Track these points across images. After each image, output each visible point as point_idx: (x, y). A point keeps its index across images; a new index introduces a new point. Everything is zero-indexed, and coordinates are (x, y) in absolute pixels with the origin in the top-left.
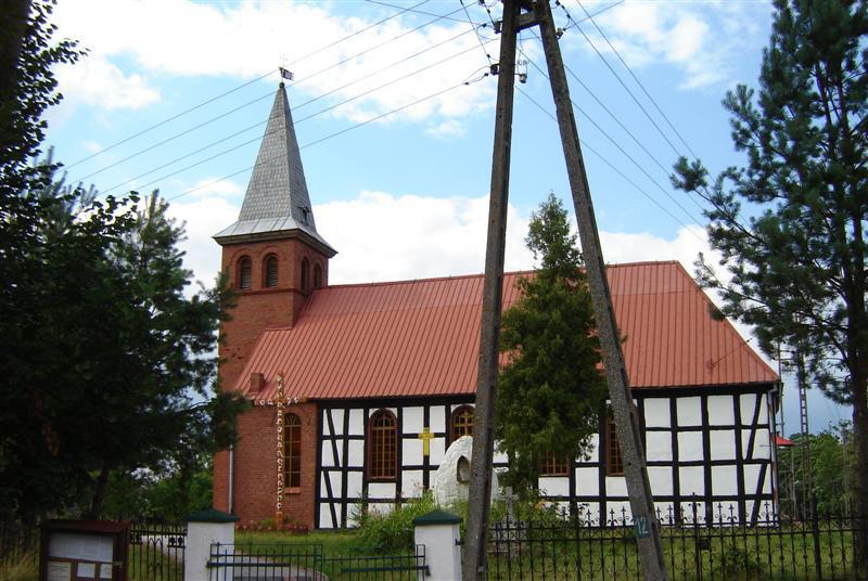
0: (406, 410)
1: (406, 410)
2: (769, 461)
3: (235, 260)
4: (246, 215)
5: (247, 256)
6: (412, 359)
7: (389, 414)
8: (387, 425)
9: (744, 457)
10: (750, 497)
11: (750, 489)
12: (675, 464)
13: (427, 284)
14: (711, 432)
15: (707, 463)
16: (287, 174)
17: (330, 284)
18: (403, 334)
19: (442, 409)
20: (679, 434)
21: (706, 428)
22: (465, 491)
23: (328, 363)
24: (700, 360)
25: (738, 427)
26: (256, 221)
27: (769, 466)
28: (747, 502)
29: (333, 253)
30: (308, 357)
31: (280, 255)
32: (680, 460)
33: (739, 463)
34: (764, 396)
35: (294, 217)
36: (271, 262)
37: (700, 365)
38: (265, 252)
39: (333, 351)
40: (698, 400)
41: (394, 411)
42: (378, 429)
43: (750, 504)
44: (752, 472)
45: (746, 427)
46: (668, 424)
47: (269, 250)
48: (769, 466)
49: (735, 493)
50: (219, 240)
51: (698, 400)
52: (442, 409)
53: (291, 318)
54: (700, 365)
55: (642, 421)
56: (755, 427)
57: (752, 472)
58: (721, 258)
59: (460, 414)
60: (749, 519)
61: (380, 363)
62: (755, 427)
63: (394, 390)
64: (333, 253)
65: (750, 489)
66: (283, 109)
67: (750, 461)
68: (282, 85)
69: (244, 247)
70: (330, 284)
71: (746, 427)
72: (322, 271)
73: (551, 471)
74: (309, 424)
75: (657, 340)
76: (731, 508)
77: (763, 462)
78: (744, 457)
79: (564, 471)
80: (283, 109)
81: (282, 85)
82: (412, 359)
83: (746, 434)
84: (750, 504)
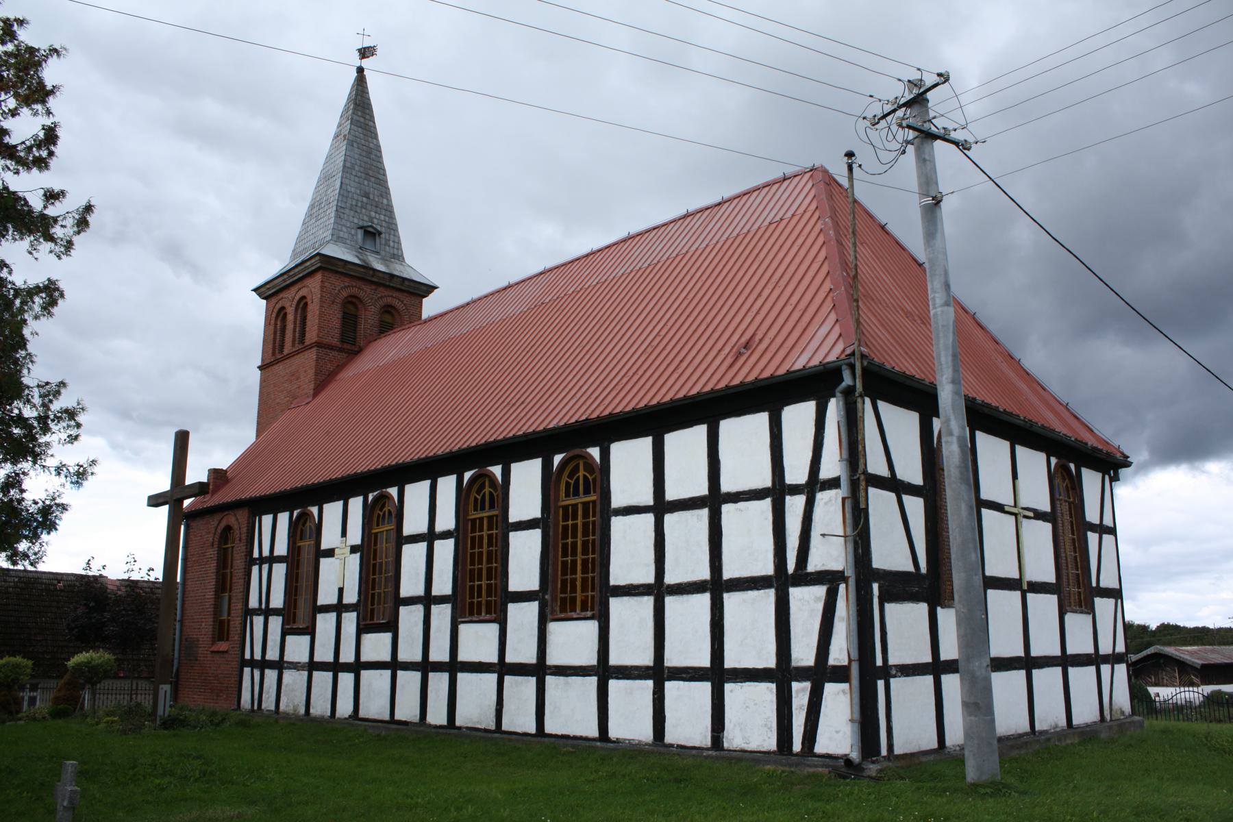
6: (495, 361)
9: (791, 566)
14: (331, 674)
23: (411, 400)
27: (842, 587)
28: (795, 686)
30: (476, 365)
32: (400, 673)
39: (509, 351)
45: (795, 490)
53: (312, 386)
56: (814, 485)
58: (53, 61)
60: (797, 746)
61: (407, 405)
62: (814, 485)
65: (804, 653)
66: (360, 102)
67: (804, 578)
68: (360, 70)
71: (795, 490)
74: (240, 540)
75: (627, 258)
76: (808, 659)
77: (830, 579)
78: (791, 566)
80: (360, 102)
81: (360, 70)
82: (495, 361)
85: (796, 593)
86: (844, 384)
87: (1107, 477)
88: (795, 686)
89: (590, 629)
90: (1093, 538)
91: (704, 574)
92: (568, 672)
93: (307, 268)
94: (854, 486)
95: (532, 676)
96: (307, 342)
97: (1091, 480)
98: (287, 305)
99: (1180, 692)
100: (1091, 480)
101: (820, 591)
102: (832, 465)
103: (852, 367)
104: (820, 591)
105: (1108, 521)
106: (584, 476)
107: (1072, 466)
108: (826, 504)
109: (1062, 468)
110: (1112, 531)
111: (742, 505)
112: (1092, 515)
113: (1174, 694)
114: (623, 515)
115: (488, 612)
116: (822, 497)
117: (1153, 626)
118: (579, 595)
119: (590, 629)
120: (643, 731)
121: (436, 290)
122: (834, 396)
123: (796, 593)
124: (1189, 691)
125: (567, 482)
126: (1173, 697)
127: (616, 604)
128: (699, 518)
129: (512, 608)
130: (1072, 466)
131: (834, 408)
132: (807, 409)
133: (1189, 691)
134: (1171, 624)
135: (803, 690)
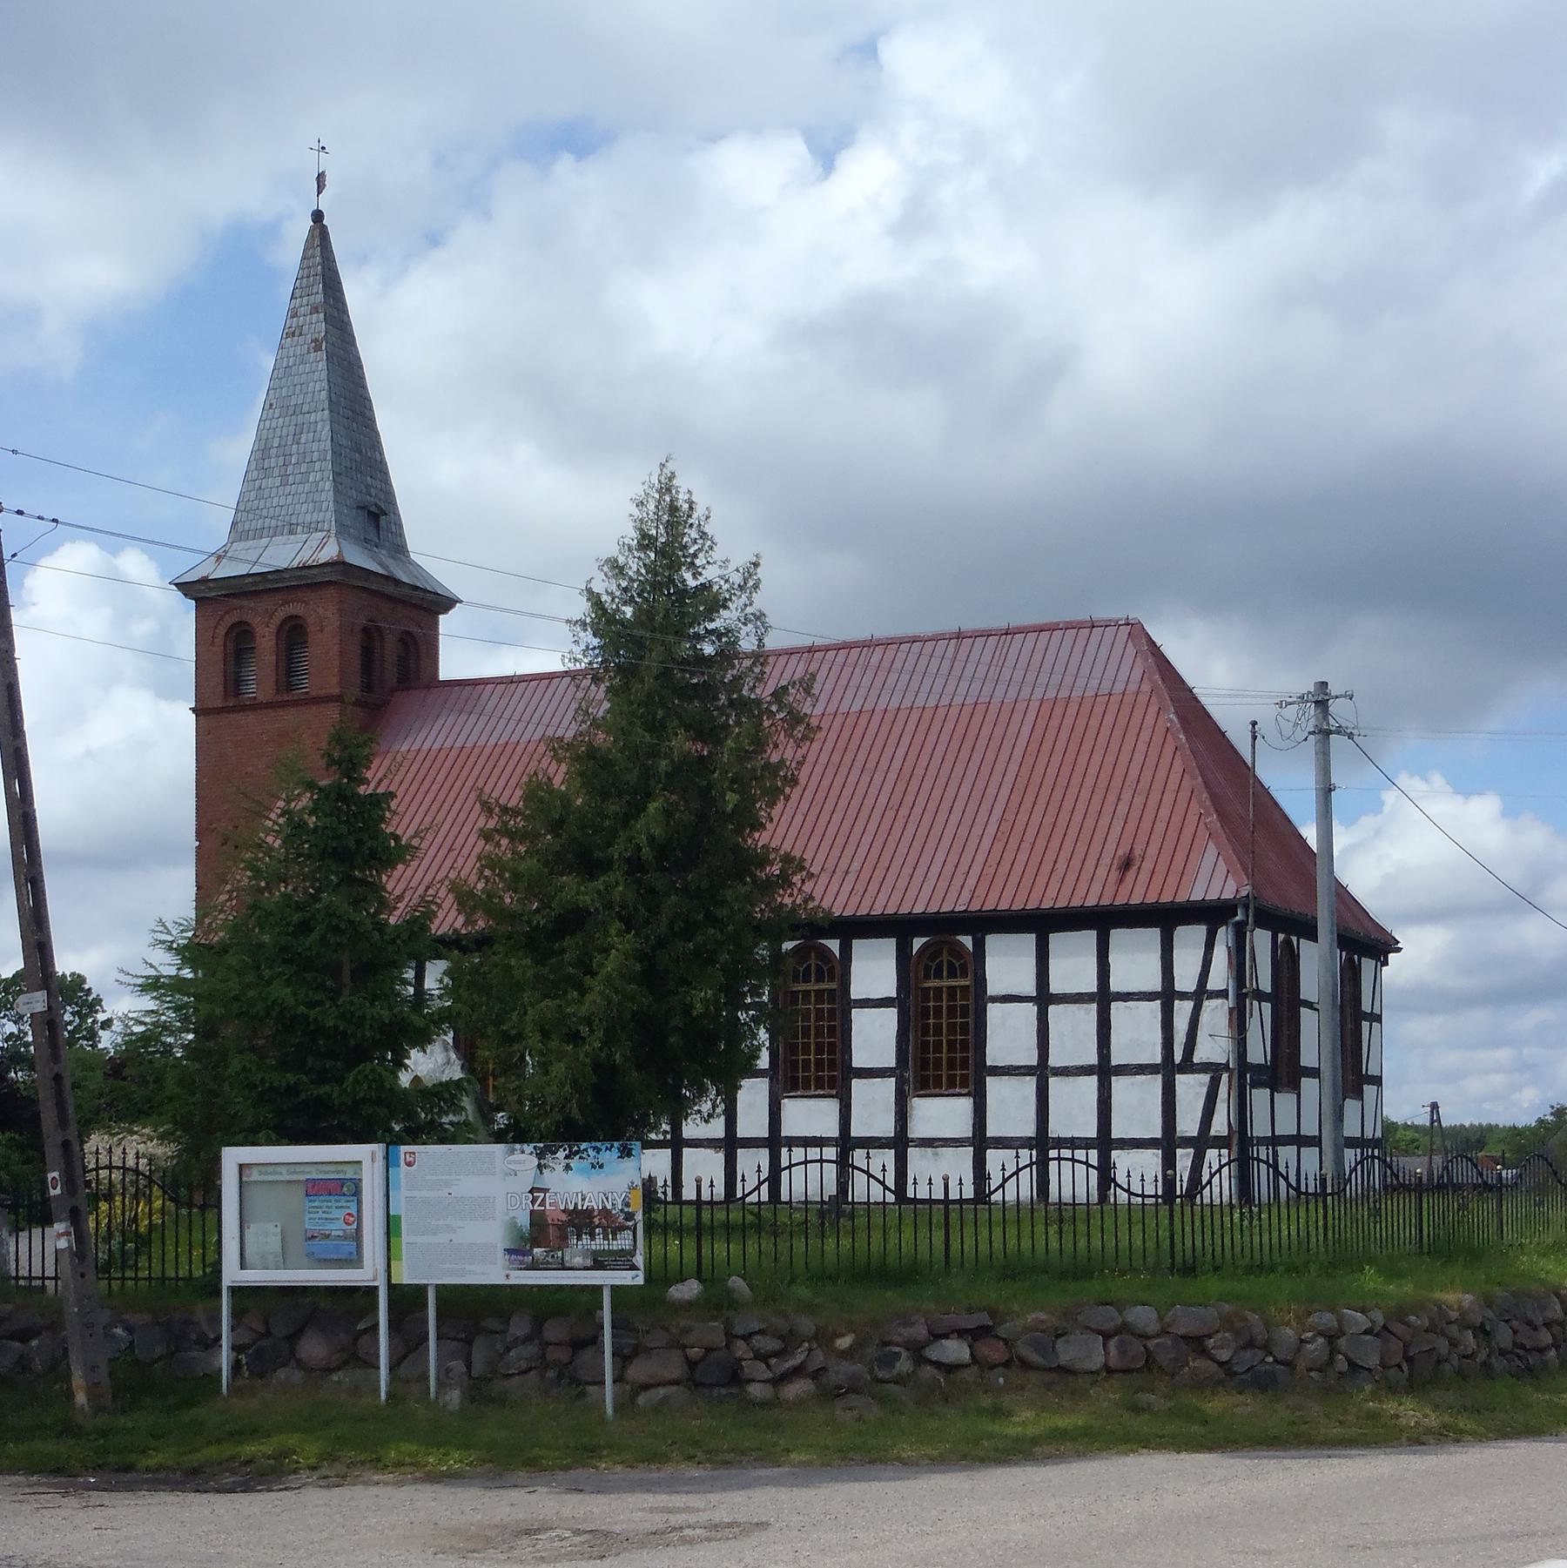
0: (992, 942)
1: (992, 942)
2: (1226, 1067)
3: (222, 631)
4: (238, 532)
5: (240, 623)
7: (958, 950)
8: (952, 975)
9: (1178, 1058)
10: (1187, 1142)
11: (1188, 1124)
12: (1042, 1072)
13: (490, 687)
15: (1105, 1071)
16: (326, 433)
17: (445, 673)
18: (1094, 723)
19: (888, 946)
20: (1052, 1008)
21: (1104, 998)
22: (430, 1085)
24: (1110, 847)
25: (1167, 995)
26: (265, 541)
27: (1225, 1077)
28: (1179, 1152)
29: (446, 603)
31: (311, 621)
33: (1168, 1070)
34: (1222, 931)
35: (342, 531)
36: (293, 634)
37: (1106, 861)
38: (281, 614)
40: (1029, 940)
41: (967, 941)
42: (933, 983)
43: (1184, 1158)
44: (1190, 1089)
45: (1184, 996)
46: (1030, 989)
47: (291, 609)
48: (1225, 1077)
49: (1156, 1132)
50: (185, 588)
51: (1029, 940)
52: (888, 946)
54: (1106, 861)
55: (981, 981)
56: (1201, 994)
57: (1190, 1089)
59: (932, 958)
62: (1201, 994)
63: (1052, 893)
64: (446, 603)
65: (1188, 1124)
67: (1188, 1066)
69: (236, 602)
70: (445, 673)
71: (1184, 996)
72: (420, 649)
73: (938, 1084)
77: (1214, 1069)
78: (1178, 1058)
79: (964, 1084)
83: (1183, 1009)
84: (1184, 1158)
85: (1181, 1080)
86: (1237, 918)
87: (1379, 964)
88: (1179, 1152)
89: (964, 1105)
90: (1365, 1025)
91: (1092, 1059)
92: (936, 1144)
93: (305, 577)
94: (1241, 998)
95: (890, 1149)
96: (306, 686)
97: (1367, 965)
98: (256, 621)
99: (806, 1162)
100: (1367, 965)
101: (1205, 1078)
102: (1219, 977)
103: (1246, 907)
104: (1205, 1078)
105: (1377, 1011)
106: (949, 961)
107: (1356, 957)
108: (1213, 1010)
109: (1350, 960)
110: (1378, 1019)
111: (1130, 1003)
112: (1366, 1007)
113: (1011, 1169)
114: (1001, 1003)
115: (831, 1087)
116: (1209, 1005)
117: (1501, 1126)
118: (944, 1073)
119: (964, 1105)
120: (913, 1196)
121: (458, 605)
122: (1227, 925)
123: (1181, 1080)
124: (1073, 1160)
125: (926, 965)
126: (1016, 1173)
127: (992, 1083)
128: (1088, 1012)
129: (856, 1084)
130: (1356, 957)
131: (1224, 936)
132: (1198, 932)
133: (1073, 1160)
134: (1508, 1125)
135: (1188, 1154)
